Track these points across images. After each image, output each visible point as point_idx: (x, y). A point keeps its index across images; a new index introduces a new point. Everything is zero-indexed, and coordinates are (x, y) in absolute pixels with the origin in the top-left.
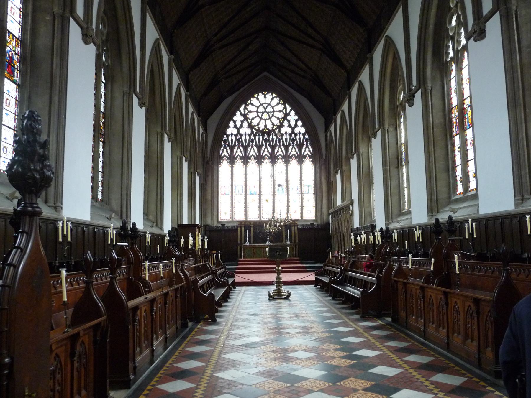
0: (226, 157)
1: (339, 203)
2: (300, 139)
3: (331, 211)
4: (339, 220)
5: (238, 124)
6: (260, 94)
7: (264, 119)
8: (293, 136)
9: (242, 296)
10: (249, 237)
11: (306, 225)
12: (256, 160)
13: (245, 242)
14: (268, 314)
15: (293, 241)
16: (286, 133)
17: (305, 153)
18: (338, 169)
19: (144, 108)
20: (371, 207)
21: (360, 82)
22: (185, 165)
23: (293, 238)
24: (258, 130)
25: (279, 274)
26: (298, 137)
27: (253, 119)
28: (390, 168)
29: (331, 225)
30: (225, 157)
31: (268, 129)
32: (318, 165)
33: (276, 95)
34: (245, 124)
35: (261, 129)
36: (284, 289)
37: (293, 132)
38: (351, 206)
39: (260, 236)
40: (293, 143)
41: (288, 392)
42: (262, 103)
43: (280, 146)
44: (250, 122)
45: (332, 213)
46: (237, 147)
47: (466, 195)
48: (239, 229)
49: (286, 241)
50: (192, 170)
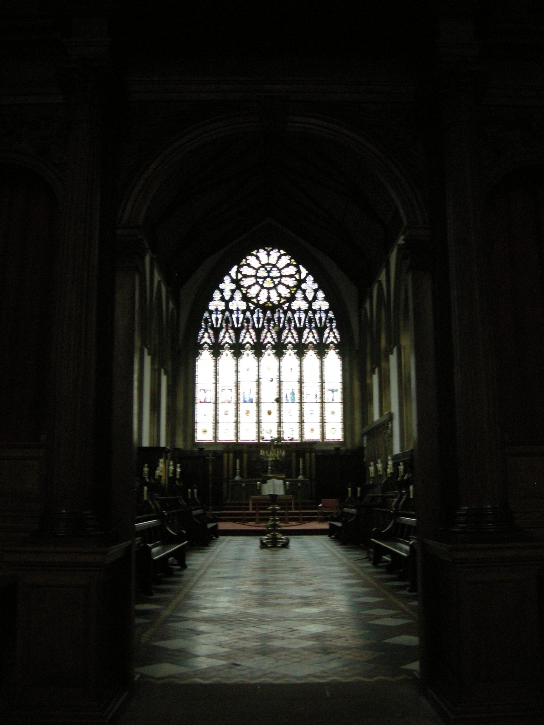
1: (376, 417)
3: (366, 429)
31: (272, 303)
32: (347, 359)
48: (225, 455)
50: (156, 367)
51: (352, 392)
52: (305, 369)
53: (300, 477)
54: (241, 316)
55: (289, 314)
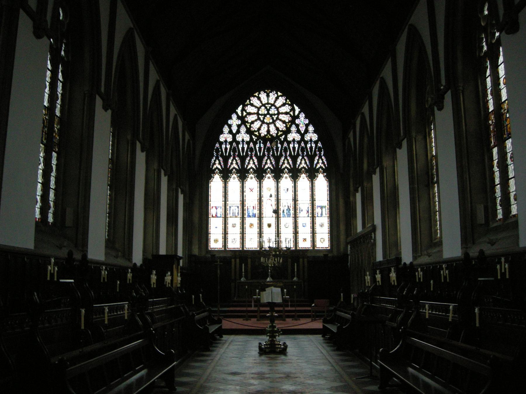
0: (219, 169)
1: (359, 229)
2: (311, 148)
3: (349, 239)
5: (234, 129)
6: (262, 93)
7: (267, 123)
8: (303, 144)
10: (246, 271)
11: (319, 257)
12: (256, 175)
13: (241, 277)
14: (252, 374)
16: (294, 140)
17: (318, 166)
18: (357, 186)
19: (109, 112)
20: (397, 236)
21: (382, 78)
22: (164, 180)
24: (259, 137)
25: (272, 321)
26: (309, 146)
27: (253, 122)
28: (418, 187)
29: (349, 257)
30: (217, 170)
31: (271, 135)
32: (333, 181)
33: (281, 94)
34: (243, 129)
35: (262, 135)
36: (281, 339)
37: (303, 139)
38: (373, 234)
40: (303, 153)
42: (263, 103)
43: (286, 157)
44: (248, 127)
45: (350, 243)
46: (232, 158)
47: (507, 222)
48: (233, 260)
53: (295, 279)
54: (246, 146)
55: (285, 144)
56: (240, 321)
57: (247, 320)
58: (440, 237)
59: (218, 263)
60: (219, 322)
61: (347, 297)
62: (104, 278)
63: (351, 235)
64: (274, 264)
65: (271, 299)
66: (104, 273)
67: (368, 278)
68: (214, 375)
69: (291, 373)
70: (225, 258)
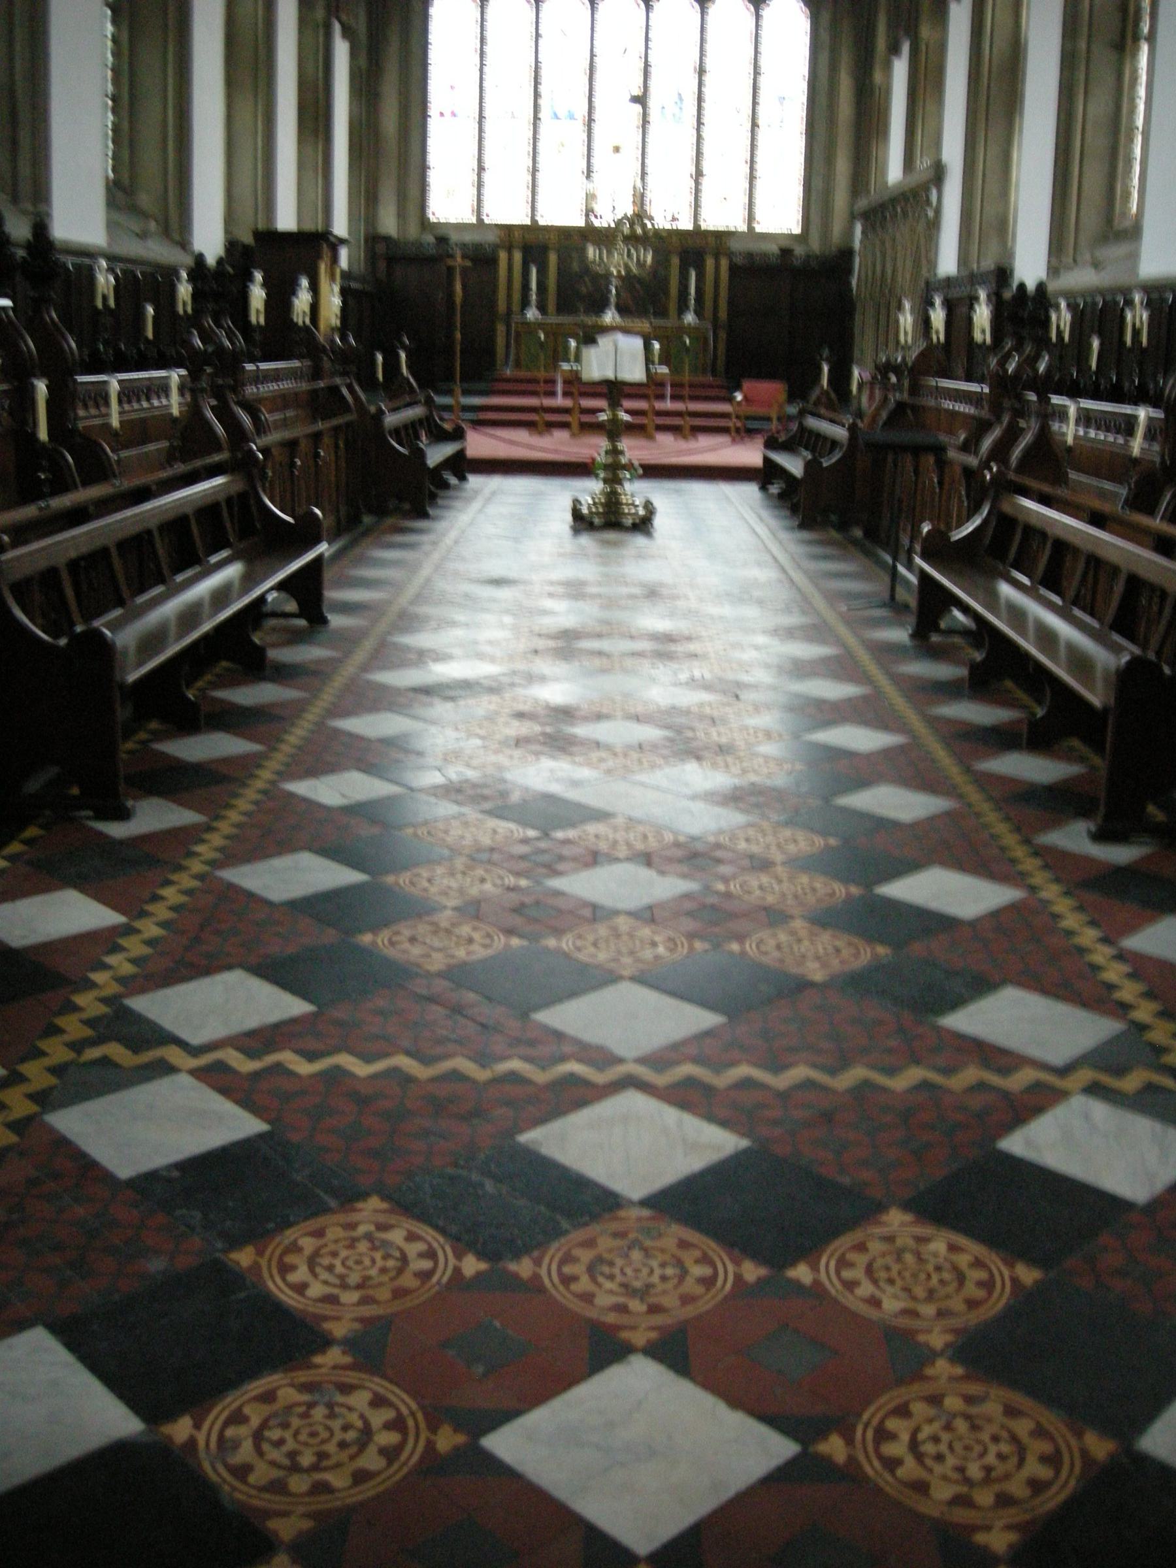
1: (894, 172)
3: (862, 204)
4: (888, 245)
9: (480, 511)
13: (525, 303)
15: (708, 312)
23: (709, 304)
32: (826, 16)
36: (636, 492)
38: (934, 192)
39: (584, 290)
41: (523, 857)
48: (503, 255)
49: (682, 308)
50: (320, 14)
51: (832, 107)
52: (710, 26)
53: (690, 318)
56: (522, 435)
57: (540, 433)
58: (1137, 215)
59: (459, 259)
60: (458, 435)
61: (841, 377)
62: (105, 298)
63: (868, 192)
64: (626, 266)
65: (611, 364)
66: (105, 281)
67: (906, 320)
68: (441, 584)
69: (661, 585)
70: (478, 247)
